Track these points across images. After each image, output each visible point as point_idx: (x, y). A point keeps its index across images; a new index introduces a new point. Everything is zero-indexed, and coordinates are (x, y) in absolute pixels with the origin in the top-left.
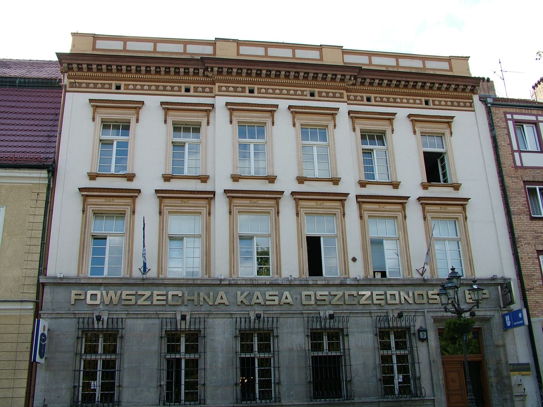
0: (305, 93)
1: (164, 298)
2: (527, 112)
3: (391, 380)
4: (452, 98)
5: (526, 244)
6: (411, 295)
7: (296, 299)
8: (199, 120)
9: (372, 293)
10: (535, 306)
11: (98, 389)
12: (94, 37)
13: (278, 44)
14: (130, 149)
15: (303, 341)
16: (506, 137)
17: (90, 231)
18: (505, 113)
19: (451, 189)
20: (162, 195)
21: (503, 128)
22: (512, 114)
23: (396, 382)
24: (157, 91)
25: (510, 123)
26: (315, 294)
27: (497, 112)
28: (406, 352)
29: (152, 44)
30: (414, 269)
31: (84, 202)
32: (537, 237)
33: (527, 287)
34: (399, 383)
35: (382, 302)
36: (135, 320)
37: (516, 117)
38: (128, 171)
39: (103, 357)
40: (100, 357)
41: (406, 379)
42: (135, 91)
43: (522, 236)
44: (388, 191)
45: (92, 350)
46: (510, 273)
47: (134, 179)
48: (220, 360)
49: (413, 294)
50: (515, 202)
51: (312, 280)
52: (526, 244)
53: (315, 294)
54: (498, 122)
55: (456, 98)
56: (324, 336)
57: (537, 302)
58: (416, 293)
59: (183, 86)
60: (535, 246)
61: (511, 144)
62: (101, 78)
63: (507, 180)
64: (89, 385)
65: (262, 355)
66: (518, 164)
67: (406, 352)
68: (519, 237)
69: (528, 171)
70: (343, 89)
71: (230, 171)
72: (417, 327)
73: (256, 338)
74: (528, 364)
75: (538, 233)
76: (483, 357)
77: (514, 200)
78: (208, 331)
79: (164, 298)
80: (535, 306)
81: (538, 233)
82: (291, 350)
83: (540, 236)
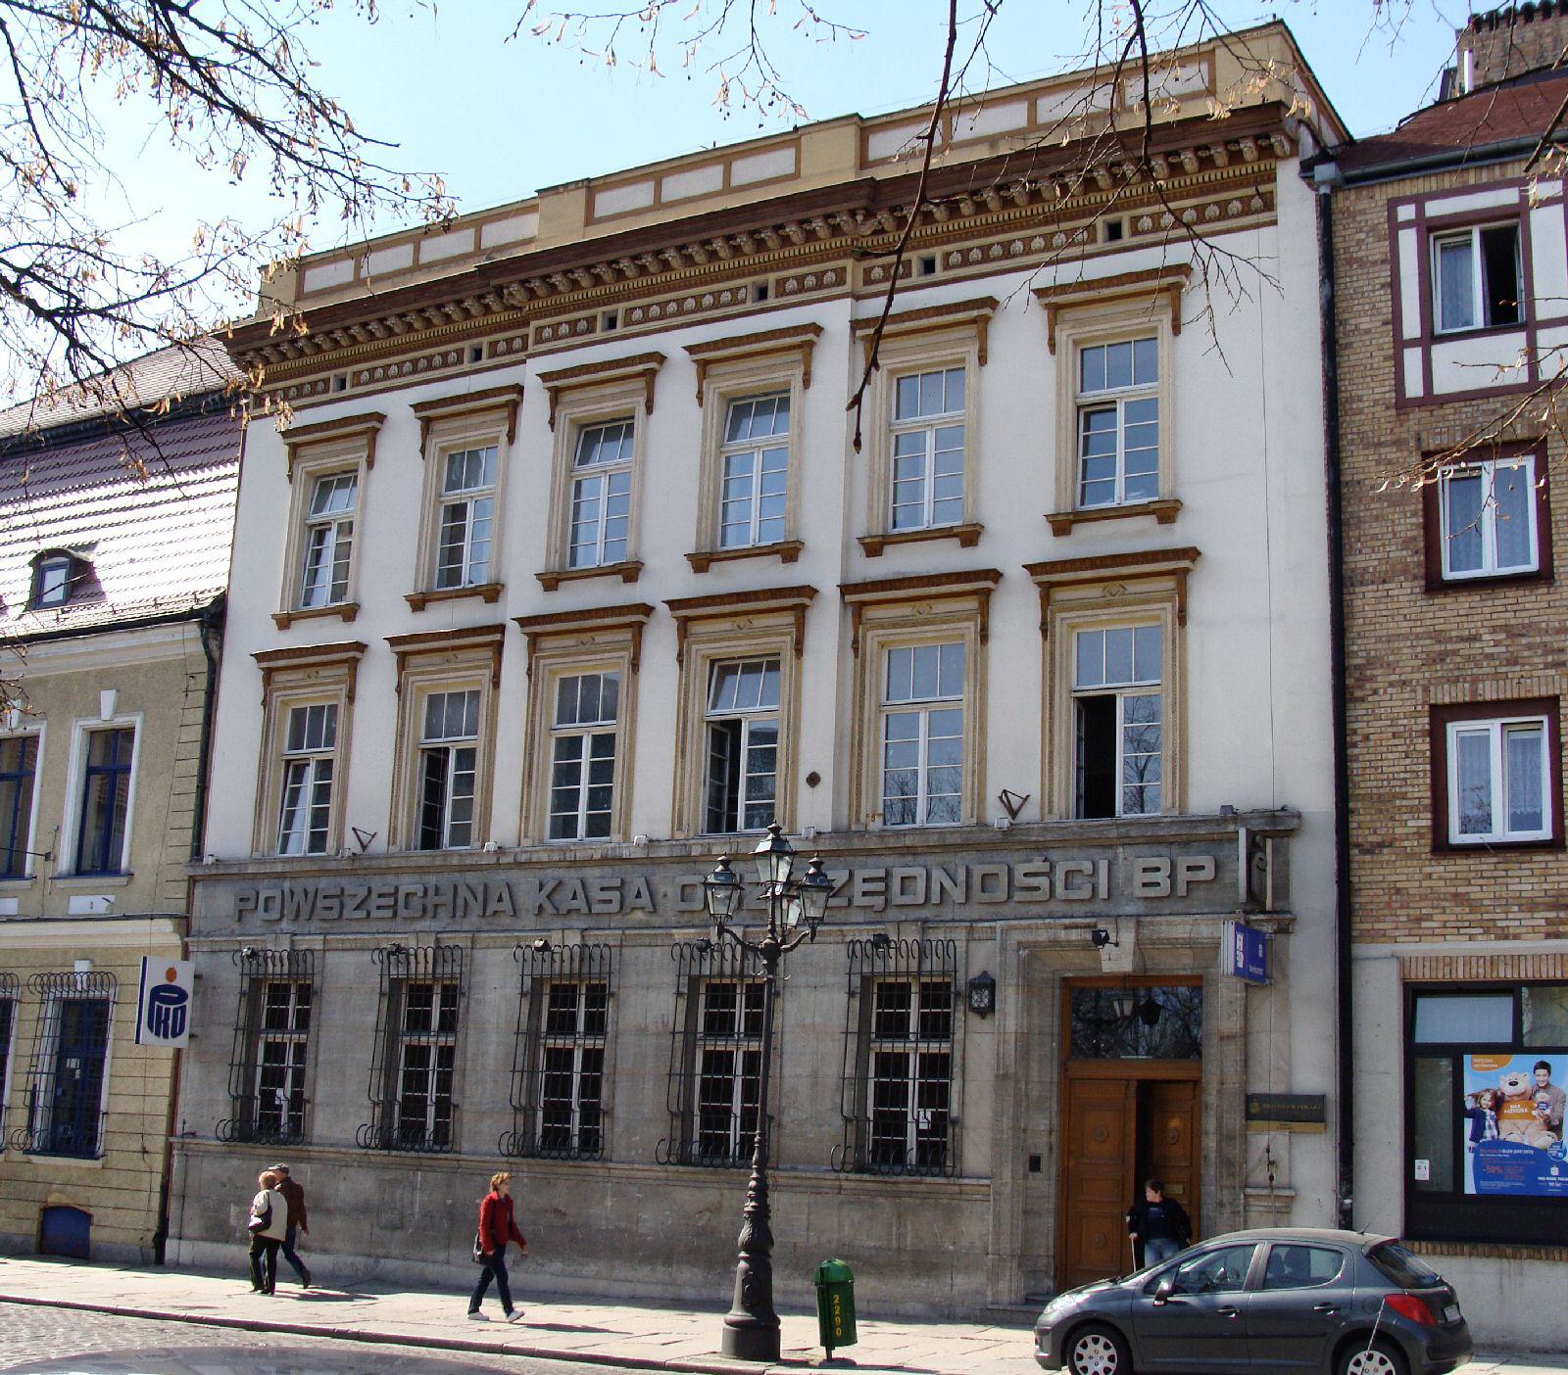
0: (741, 294)
1: (881, 887)
2: (1485, 177)
3: (898, 1124)
4: (505, 329)
5: (1391, 684)
6: (961, 877)
7: (665, 895)
8: (778, 377)
9: (851, 874)
10: (1388, 905)
11: (285, 1105)
12: (588, 188)
13: (685, 161)
14: (1163, 422)
15: (672, 1008)
16: (1384, 297)
17: (1068, 682)
18: (1393, 204)
19: (1150, 521)
20: (1048, 577)
21: (1374, 263)
22: (1419, 201)
23: (911, 1129)
24: (1007, 260)
25: (1408, 240)
26: (1010, 871)
27: (1360, 206)
28: (550, 1042)
29: (649, 186)
30: (992, 794)
31: (1046, 601)
32: (1441, 657)
33: (1357, 835)
34: (920, 1133)
35: (879, 901)
36: (340, 954)
37: (1435, 209)
38: (1164, 491)
39: (923, 1047)
40: (914, 1049)
41: (940, 1124)
42: (967, 266)
43: (1380, 658)
44: (947, 557)
45: (893, 1027)
46: (1315, 797)
47: (801, 555)
48: (492, 1049)
49: (968, 872)
50: (1374, 537)
51: (424, 857)
52: (1391, 684)
53: (1010, 871)
54: (1360, 242)
55: (404, 352)
56: (738, 997)
57: (1398, 891)
58: (978, 871)
59: (1100, 222)
60: (1426, 690)
61: (1396, 320)
62: (724, 274)
63: (1358, 461)
64: (273, 1094)
65: (899, 1047)
66: (1414, 388)
67: (550, 1042)
68: (1371, 663)
69: (1448, 409)
70: (845, 256)
71: (689, 541)
72: (975, 972)
73: (583, 998)
74: (1321, 1099)
75: (1450, 640)
76: (1064, 1067)
77: (1376, 528)
78: (476, 979)
79: (881, 887)
80: (1388, 905)
81: (1450, 640)
82: (643, 1031)
83: (1455, 653)
